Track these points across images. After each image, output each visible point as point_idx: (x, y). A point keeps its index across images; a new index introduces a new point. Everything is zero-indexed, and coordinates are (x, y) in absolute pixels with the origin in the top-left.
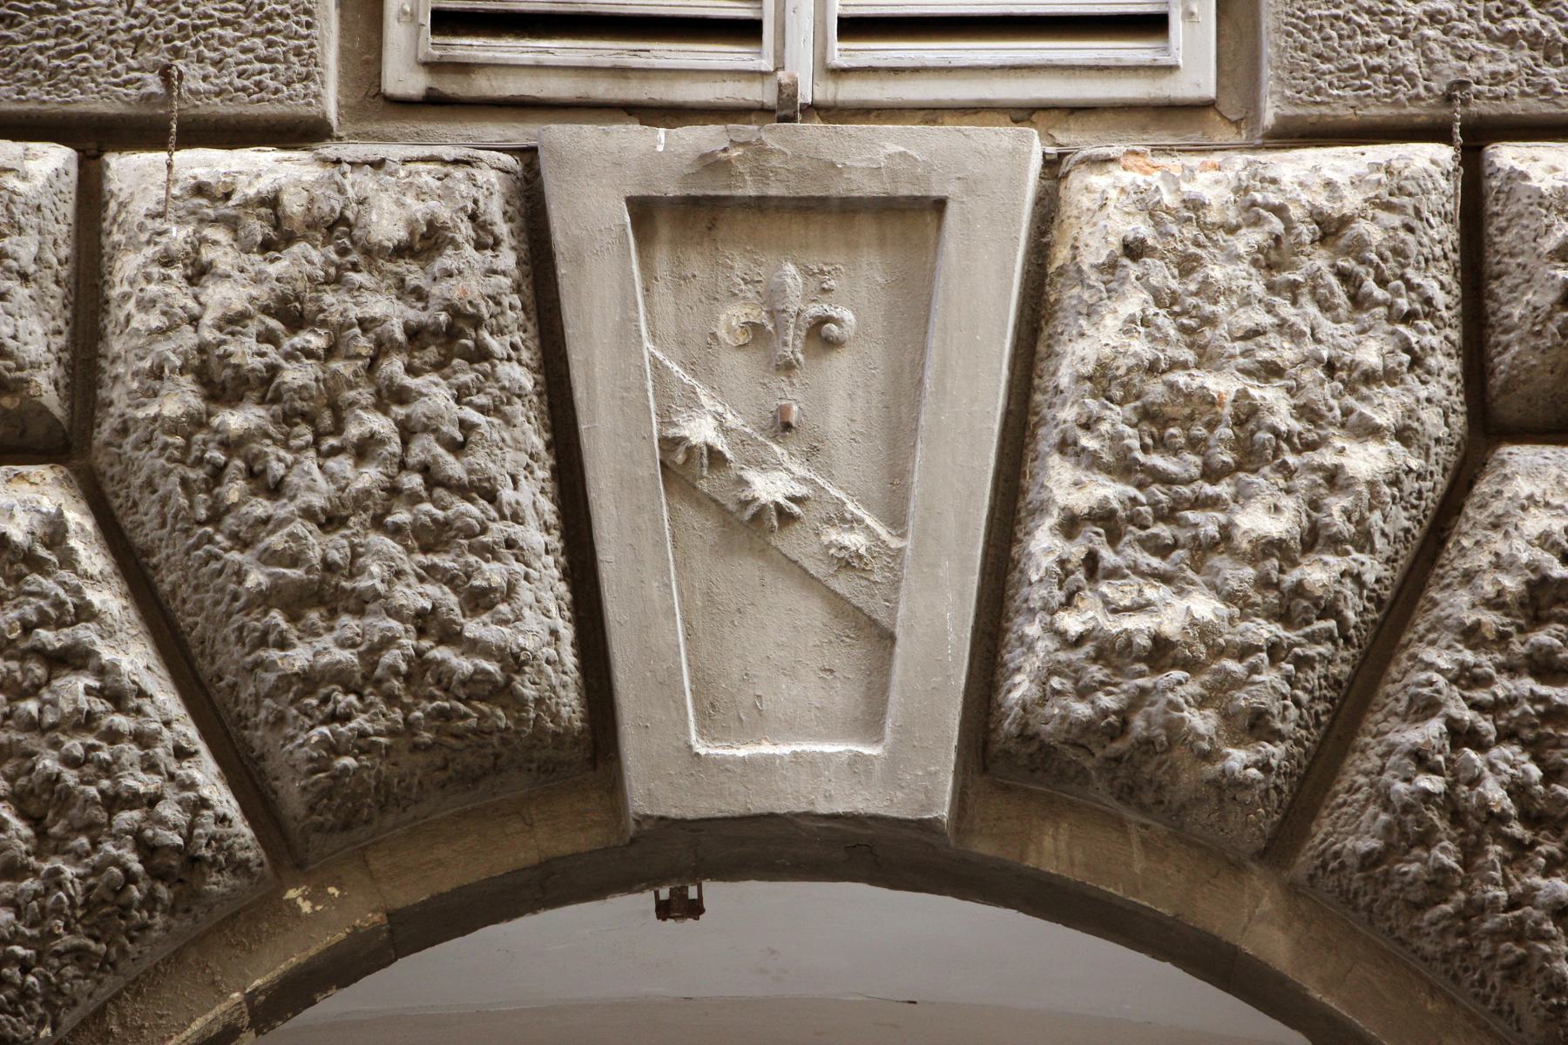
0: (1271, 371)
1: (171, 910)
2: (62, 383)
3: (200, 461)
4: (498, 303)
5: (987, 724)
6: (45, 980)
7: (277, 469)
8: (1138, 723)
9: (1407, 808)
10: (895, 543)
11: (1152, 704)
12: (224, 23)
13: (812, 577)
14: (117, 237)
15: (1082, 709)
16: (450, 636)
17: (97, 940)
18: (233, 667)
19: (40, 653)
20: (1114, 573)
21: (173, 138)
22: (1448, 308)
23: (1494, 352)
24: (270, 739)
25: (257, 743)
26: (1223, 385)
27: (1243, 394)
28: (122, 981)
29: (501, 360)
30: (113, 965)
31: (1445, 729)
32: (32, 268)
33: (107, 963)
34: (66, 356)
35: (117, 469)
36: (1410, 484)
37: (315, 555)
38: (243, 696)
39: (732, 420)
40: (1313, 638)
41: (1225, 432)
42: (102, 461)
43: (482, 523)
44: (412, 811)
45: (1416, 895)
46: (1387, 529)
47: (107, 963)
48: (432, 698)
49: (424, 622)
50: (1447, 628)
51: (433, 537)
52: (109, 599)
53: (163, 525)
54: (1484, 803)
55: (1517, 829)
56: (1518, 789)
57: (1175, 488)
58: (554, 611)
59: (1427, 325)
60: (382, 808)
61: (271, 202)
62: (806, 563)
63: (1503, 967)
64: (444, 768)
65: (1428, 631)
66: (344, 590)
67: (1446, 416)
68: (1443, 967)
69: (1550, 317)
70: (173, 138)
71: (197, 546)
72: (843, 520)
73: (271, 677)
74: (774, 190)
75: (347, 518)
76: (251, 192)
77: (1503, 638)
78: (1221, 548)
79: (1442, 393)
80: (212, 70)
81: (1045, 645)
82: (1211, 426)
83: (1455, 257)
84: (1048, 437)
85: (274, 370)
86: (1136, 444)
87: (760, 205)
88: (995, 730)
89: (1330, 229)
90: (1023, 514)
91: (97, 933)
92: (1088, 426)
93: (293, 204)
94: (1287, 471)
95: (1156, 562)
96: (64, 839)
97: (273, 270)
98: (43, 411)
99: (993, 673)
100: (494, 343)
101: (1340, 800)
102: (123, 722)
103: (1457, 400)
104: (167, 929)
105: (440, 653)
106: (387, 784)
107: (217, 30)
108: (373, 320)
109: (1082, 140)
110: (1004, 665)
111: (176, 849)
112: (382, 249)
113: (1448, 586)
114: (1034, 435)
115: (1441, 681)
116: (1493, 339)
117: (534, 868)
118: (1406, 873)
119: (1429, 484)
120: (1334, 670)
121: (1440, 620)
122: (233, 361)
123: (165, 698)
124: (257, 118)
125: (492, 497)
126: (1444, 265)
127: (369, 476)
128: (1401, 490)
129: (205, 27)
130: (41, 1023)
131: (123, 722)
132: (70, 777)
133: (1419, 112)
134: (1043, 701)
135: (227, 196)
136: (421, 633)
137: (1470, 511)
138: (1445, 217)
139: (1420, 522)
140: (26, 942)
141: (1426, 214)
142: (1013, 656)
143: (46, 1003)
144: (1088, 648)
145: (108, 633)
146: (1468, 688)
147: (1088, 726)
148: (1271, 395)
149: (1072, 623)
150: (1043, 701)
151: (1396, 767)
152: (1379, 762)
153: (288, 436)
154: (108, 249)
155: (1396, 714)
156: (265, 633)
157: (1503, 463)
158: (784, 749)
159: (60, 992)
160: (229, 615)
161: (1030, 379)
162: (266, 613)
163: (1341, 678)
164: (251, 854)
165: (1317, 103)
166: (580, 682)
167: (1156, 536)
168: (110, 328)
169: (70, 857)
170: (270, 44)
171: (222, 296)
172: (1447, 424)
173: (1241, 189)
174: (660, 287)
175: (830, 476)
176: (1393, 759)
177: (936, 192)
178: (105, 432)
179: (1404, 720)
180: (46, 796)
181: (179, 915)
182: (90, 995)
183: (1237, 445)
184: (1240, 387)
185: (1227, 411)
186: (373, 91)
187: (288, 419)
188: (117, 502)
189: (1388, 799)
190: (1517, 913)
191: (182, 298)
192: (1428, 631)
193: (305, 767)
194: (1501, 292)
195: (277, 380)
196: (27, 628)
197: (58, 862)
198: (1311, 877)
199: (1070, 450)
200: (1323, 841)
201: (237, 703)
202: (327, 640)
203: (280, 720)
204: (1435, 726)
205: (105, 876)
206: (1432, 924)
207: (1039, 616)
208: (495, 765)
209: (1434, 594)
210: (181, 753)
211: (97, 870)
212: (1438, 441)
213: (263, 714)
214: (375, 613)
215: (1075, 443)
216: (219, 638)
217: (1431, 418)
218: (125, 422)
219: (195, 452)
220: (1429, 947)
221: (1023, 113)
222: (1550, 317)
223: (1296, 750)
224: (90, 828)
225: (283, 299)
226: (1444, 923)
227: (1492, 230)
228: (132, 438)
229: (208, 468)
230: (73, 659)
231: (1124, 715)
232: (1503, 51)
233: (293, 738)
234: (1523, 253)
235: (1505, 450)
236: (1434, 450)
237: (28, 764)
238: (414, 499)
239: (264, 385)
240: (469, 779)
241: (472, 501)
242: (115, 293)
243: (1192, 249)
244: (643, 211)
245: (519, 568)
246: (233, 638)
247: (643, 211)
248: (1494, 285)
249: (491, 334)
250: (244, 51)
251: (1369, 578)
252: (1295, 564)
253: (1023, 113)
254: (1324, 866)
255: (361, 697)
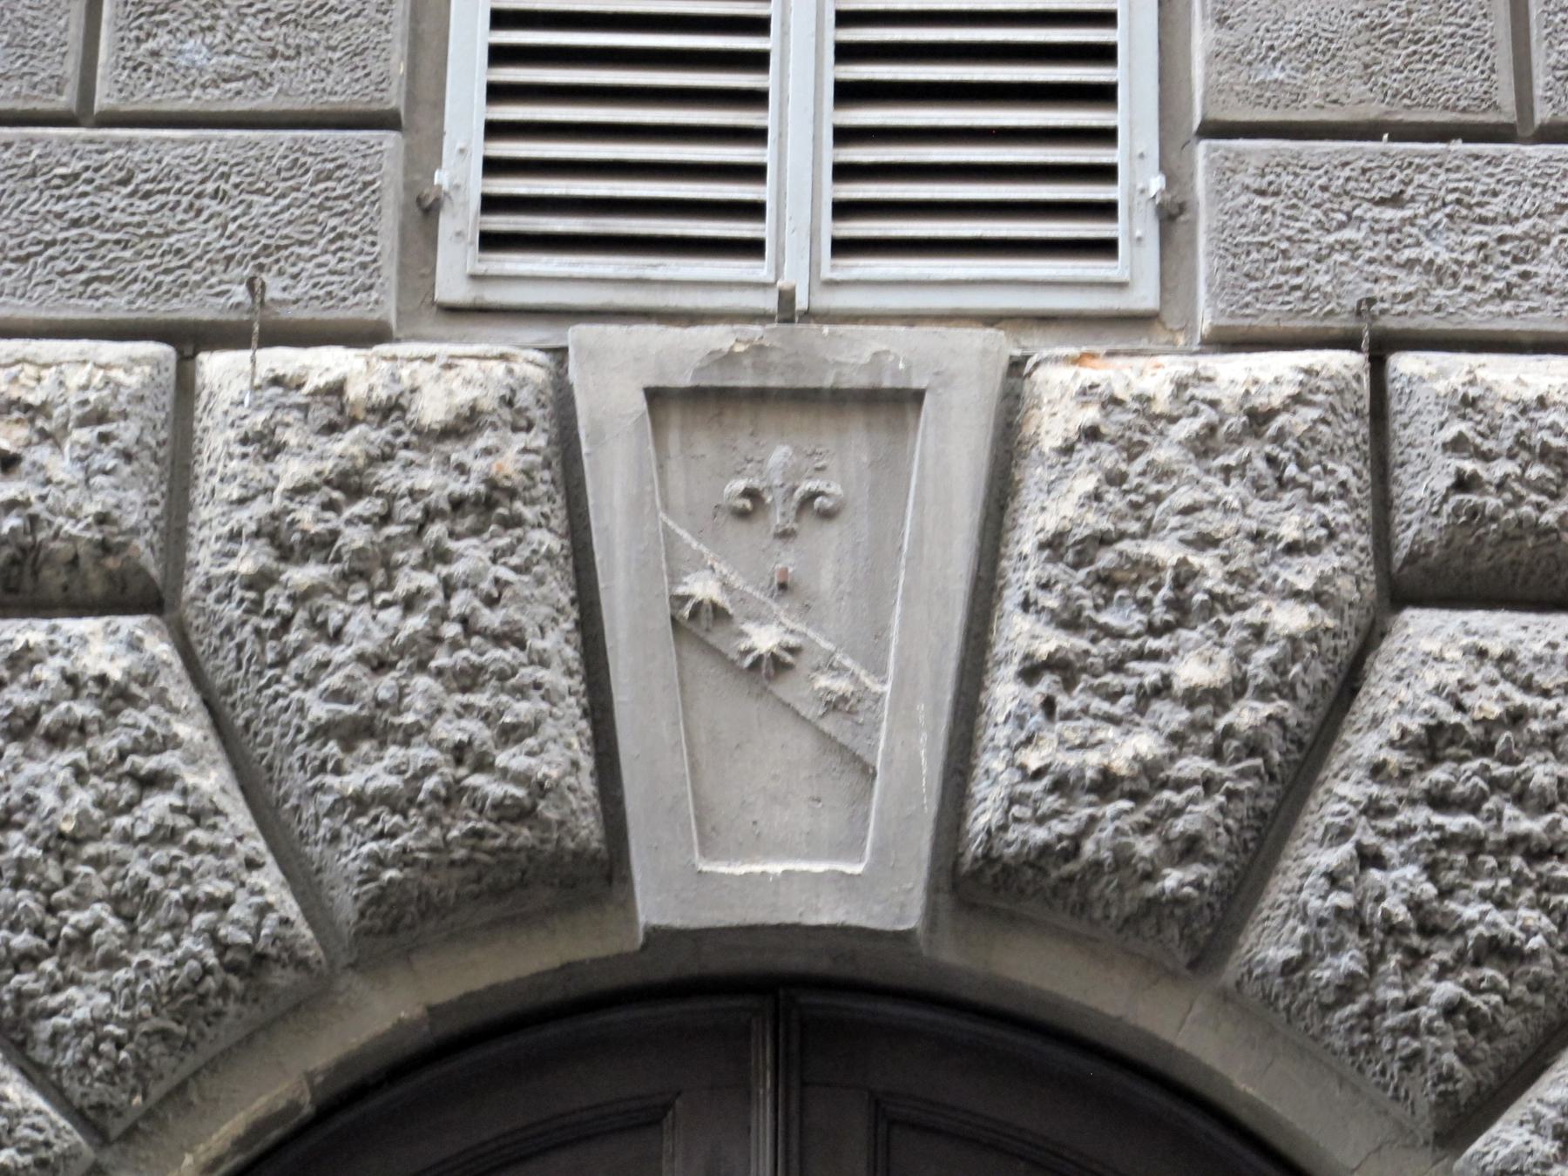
0: (1205, 542)
1: (242, 999)
2: (157, 548)
3: (270, 614)
4: (531, 478)
5: (956, 848)
6: (136, 1056)
7: (335, 619)
8: (1088, 847)
9: (1321, 922)
10: (877, 688)
11: (1101, 830)
12: (302, 243)
13: (804, 719)
14: (207, 422)
15: (1040, 835)
16: (483, 764)
17: (179, 1023)
18: (296, 792)
19: (133, 775)
20: (1068, 716)
21: (255, 339)
22: (1360, 491)
23: (1398, 530)
24: (328, 853)
25: (316, 857)
26: (1166, 551)
27: (1183, 562)
28: (201, 1061)
29: (533, 527)
30: (194, 1045)
31: (1355, 853)
32: (135, 449)
33: (188, 1043)
34: (161, 524)
35: (201, 621)
36: (1327, 642)
37: (367, 694)
38: (304, 816)
39: (737, 581)
40: (1243, 775)
41: (1165, 592)
42: (190, 613)
43: (513, 667)
44: (450, 919)
45: (1329, 998)
46: (1307, 680)
47: (188, 1043)
48: (468, 819)
49: (459, 752)
50: (1358, 766)
51: (469, 679)
52: (192, 730)
53: (239, 667)
54: (1387, 916)
55: (1415, 940)
56: (1415, 905)
57: (1123, 642)
58: (576, 746)
59: (1339, 504)
60: (423, 915)
61: (336, 390)
62: (798, 706)
63: (1401, 1059)
64: (478, 880)
65: (1342, 768)
66: (392, 725)
67: (1358, 583)
68: (1350, 1060)
69: (1445, 499)
70: (255, 339)
71: (268, 686)
72: (831, 667)
73: (328, 799)
74: (774, 382)
75: (396, 663)
76: (321, 382)
77: (1405, 775)
78: (1164, 694)
79: (1355, 564)
80: (288, 282)
81: (1008, 777)
82: (1156, 588)
83: (1366, 448)
84: (1011, 599)
85: (335, 534)
86: (1088, 603)
87: (760, 396)
88: (962, 854)
89: (1258, 419)
90: (990, 665)
91: (179, 1017)
92: (1046, 586)
93: (355, 392)
94: (1222, 629)
95: (1106, 706)
96: (151, 936)
97: (338, 448)
98: (141, 571)
99: (962, 804)
100: (529, 513)
101: (1265, 914)
102: (201, 836)
103: (1368, 570)
104: (239, 1016)
105: (477, 780)
106: (427, 893)
107: (296, 249)
108: (422, 492)
109: (1040, 345)
110: (972, 796)
111: (247, 948)
112: (431, 432)
113: (1359, 730)
114: (1000, 596)
115: (1353, 812)
116: (1397, 520)
117: (556, 971)
118: (1320, 979)
119: (1343, 642)
120: (1261, 803)
121: (1351, 759)
122: (300, 526)
123: (240, 817)
124: (329, 322)
125: (521, 644)
126: (1357, 454)
127: (417, 622)
128: (1319, 646)
129: (286, 247)
130: (133, 1092)
131: (201, 836)
132: (156, 882)
133: (1336, 324)
134: (1004, 828)
135: (299, 387)
136: (459, 762)
137: (1378, 666)
138: (1357, 414)
139: (1335, 675)
140: (120, 1022)
141: (1341, 411)
142: (980, 788)
143: (138, 1075)
144: (1046, 781)
145: (192, 760)
146: (1375, 817)
147: (1045, 849)
148: (1205, 561)
149: (1033, 760)
150: (1004, 828)
151: (1313, 886)
152: (1298, 883)
153: (345, 592)
154: (199, 433)
155: (1313, 841)
156: (324, 762)
157: (1406, 625)
158: (776, 868)
159: (148, 1066)
160: (293, 745)
161: (997, 550)
162: (325, 744)
163: (1267, 810)
164: (311, 953)
165: (1247, 316)
166: (598, 808)
167: (1106, 684)
168: (198, 500)
169: (158, 951)
170: (341, 260)
171: (292, 470)
172: (1358, 589)
173: (1181, 386)
174: (674, 466)
175: (819, 629)
176: (1310, 879)
177: (916, 384)
178: (191, 589)
179: (1321, 845)
180: (137, 899)
181: (249, 1003)
182: (174, 1071)
183: (1170, 604)
184: (1181, 555)
185: (1168, 576)
186: (428, 300)
187: (347, 577)
188: (200, 649)
189: (1306, 914)
190: (1413, 1012)
191: (259, 473)
192: (1342, 768)
193: (358, 878)
194: (1404, 478)
195: (339, 543)
196: (123, 756)
197: (145, 955)
198: (1239, 984)
199: (1032, 609)
200: (1249, 951)
201: (299, 821)
202: (377, 768)
203: (335, 837)
204: (1347, 848)
205: (186, 969)
206: (1341, 1022)
207: (1002, 754)
208: (522, 880)
209: (1347, 736)
210: (252, 864)
211: (179, 963)
212: (1351, 605)
213: (322, 832)
214: (419, 745)
215: (1036, 603)
216: (286, 766)
217: (1345, 584)
218: (209, 580)
219: (267, 606)
220: (1338, 1043)
221: (991, 319)
222: (1445, 499)
223: (1226, 872)
224: (173, 926)
225: (345, 474)
226: (1352, 1022)
227: (1396, 426)
228: (215, 593)
229: (278, 619)
230: (152, 782)
231: (1077, 839)
232: (1401, 274)
233: (347, 853)
234: (1422, 445)
235: (1409, 614)
236: (1347, 612)
237: (122, 872)
238: (455, 646)
239: (321, 545)
240: (497, 892)
241: (505, 648)
242: (202, 470)
243: (1137, 436)
244: (656, 397)
245: (544, 706)
246: (297, 765)
247: (656, 397)
248: (1397, 471)
249: (525, 504)
250: (320, 266)
251: (1292, 722)
252: (1226, 709)
253: (991, 319)
254: (1250, 972)
255: (406, 817)
